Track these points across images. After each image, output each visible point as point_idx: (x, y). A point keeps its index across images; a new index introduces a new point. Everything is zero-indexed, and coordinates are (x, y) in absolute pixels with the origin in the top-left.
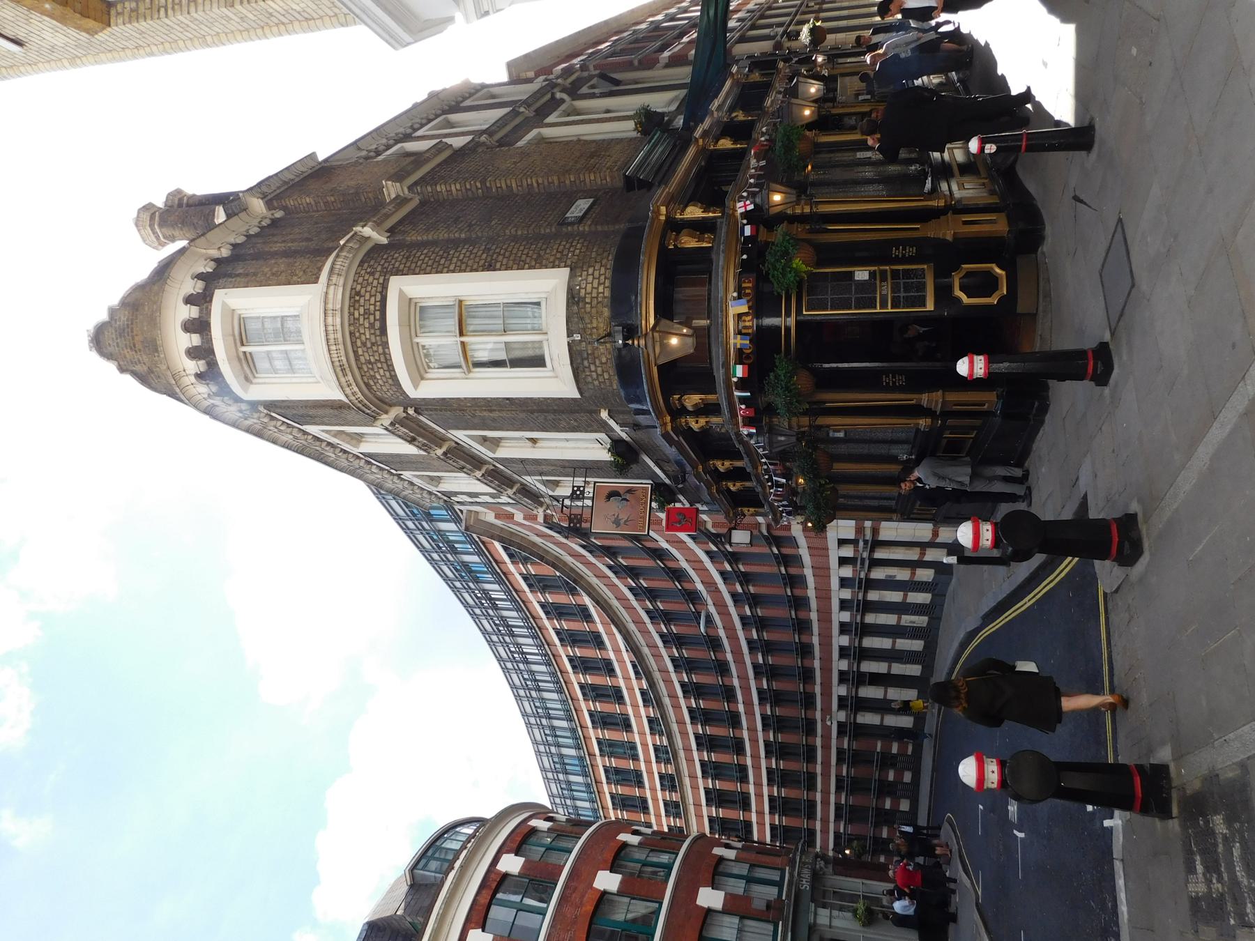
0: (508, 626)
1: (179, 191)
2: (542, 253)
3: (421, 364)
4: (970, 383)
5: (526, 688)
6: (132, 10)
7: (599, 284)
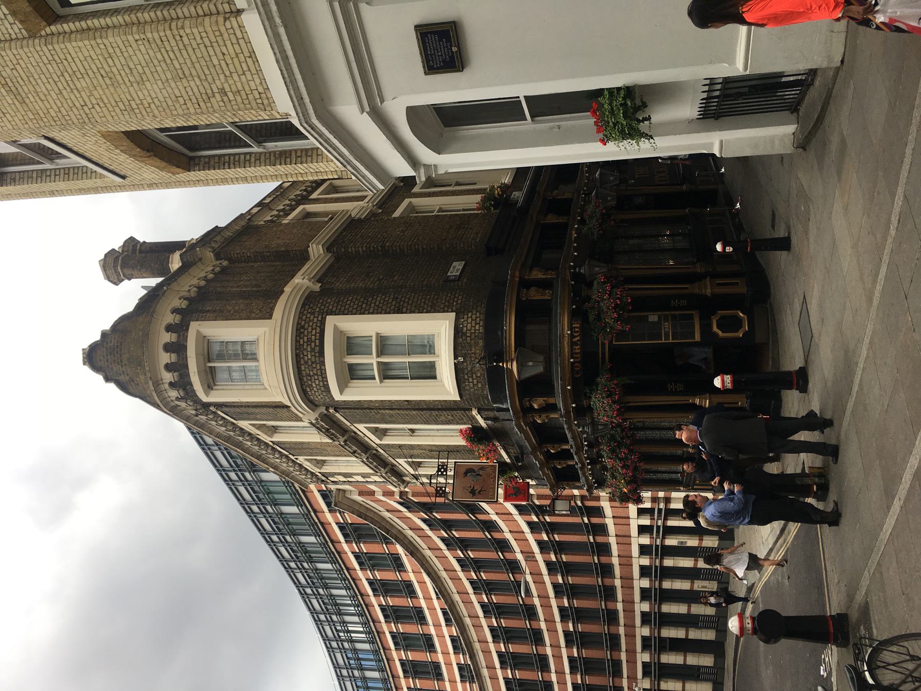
0: (336, 604)
2: (435, 302)
3: (352, 374)
4: (724, 391)
5: (349, 667)
6: (205, 163)
7: (476, 324)
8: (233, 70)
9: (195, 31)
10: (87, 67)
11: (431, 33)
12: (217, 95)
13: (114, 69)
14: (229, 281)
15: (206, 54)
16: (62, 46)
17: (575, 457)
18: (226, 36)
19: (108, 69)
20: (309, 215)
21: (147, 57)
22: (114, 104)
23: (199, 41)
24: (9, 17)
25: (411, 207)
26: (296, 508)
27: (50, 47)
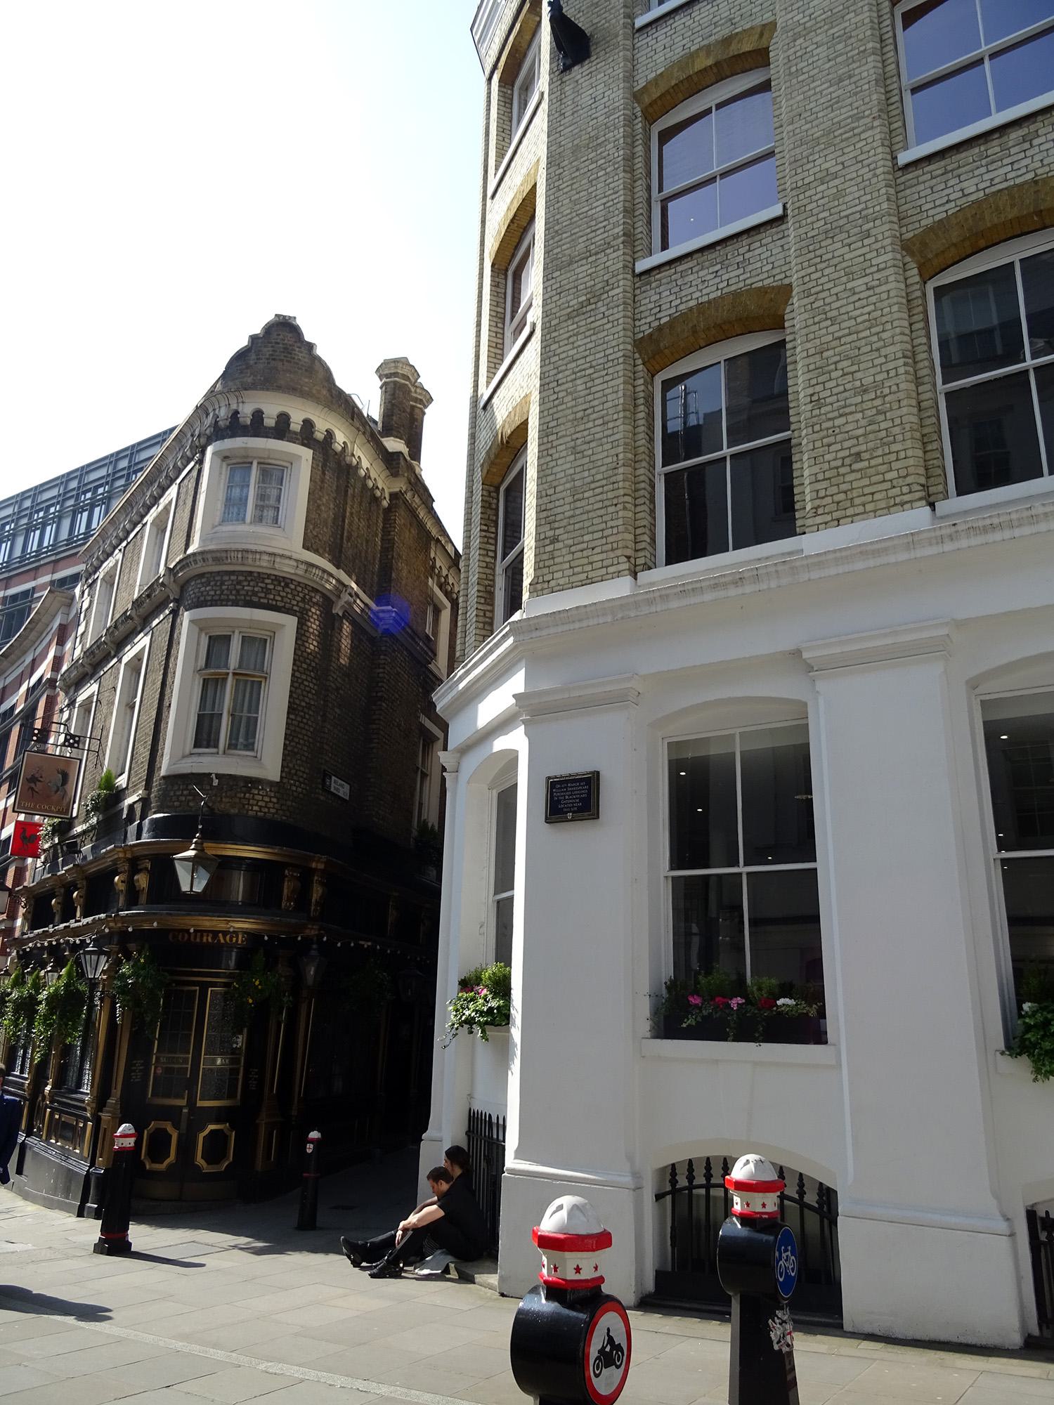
1: (430, 400)
8: (576, 556)
9: (620, 522)
10: (597, 395)
11: (589, 790)
12: (551, 533)
13: (591, 424)
14: (360, 504)
15: (595, 528)
16: (621, 374)
17: (90, 919)
18: (612, 555)
19: (593, 417)
20: (437, 611)
21: (600, 463)
22: (556, 416)
23: (609, 524)
24: (656, 323)
25: (405, 1230)
26: (66, 537)
27: (621, 360)
